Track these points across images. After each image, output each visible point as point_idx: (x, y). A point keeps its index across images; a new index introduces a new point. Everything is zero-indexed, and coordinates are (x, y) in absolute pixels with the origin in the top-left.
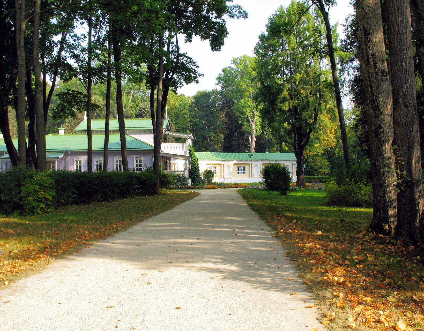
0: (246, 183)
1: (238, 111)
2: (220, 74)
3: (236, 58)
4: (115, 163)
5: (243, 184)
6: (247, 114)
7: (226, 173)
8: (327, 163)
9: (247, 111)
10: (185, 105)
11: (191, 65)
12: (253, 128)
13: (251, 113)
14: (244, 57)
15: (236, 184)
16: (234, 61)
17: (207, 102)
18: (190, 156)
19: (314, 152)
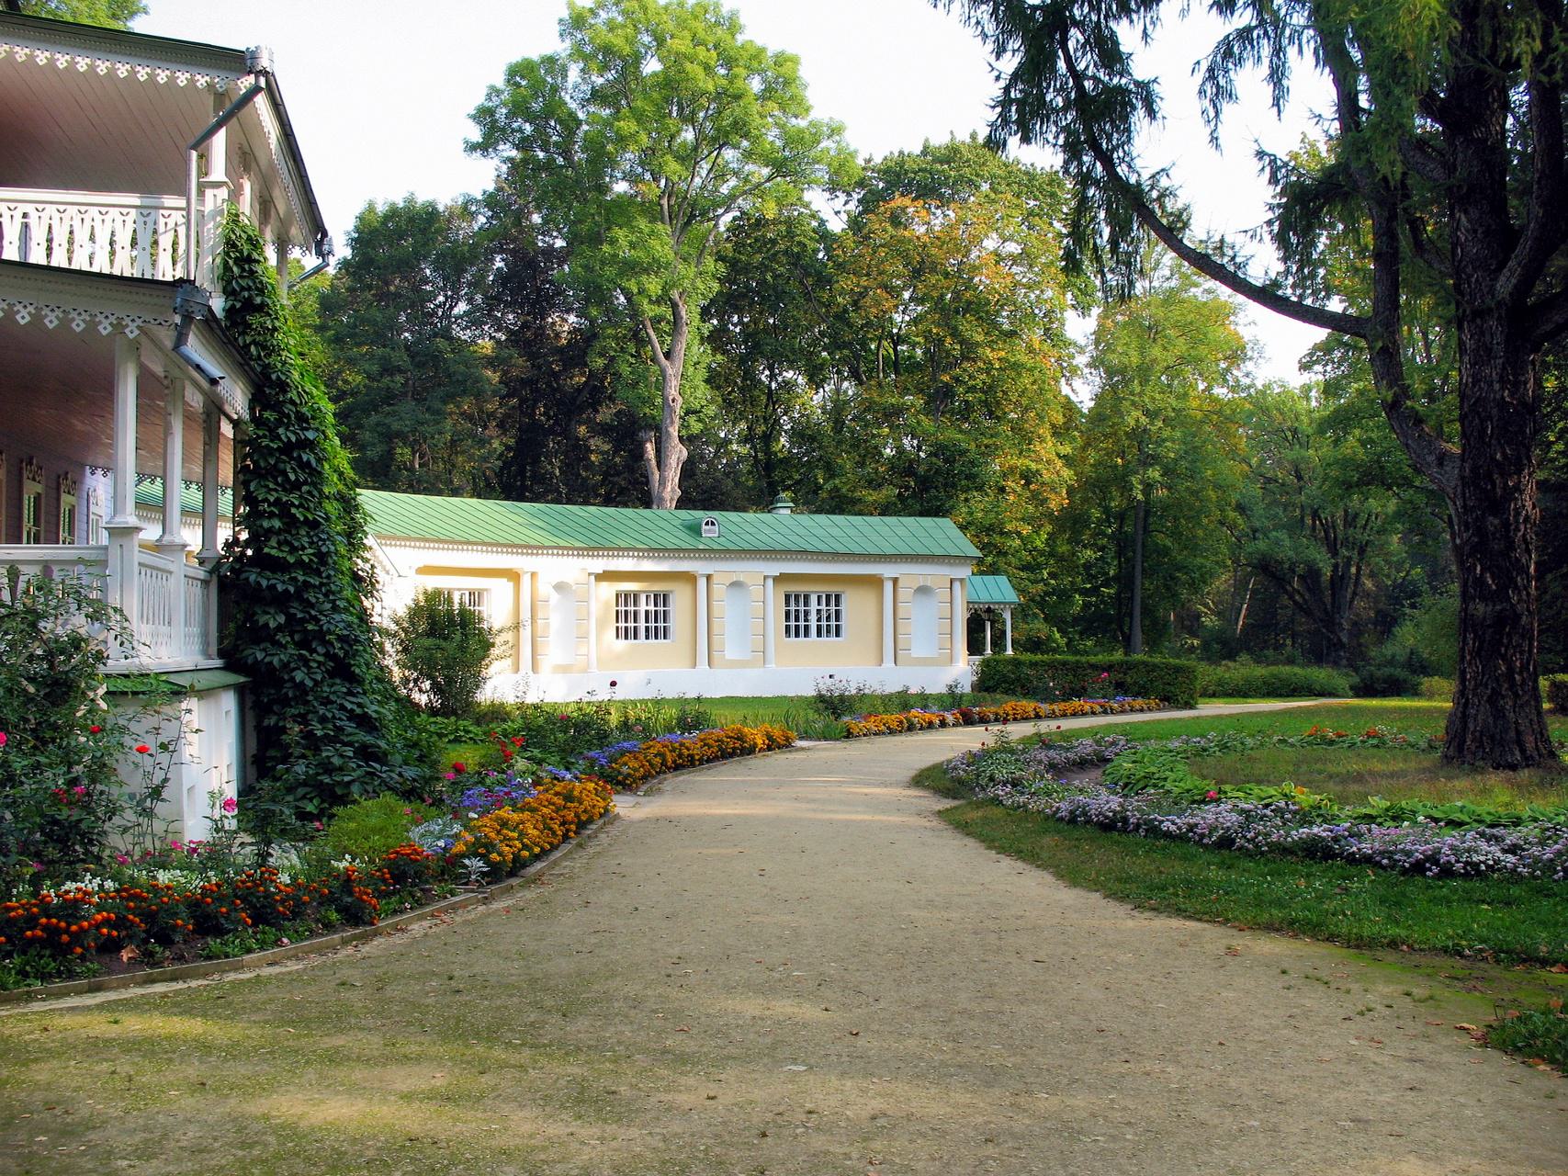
12: (673, 392)
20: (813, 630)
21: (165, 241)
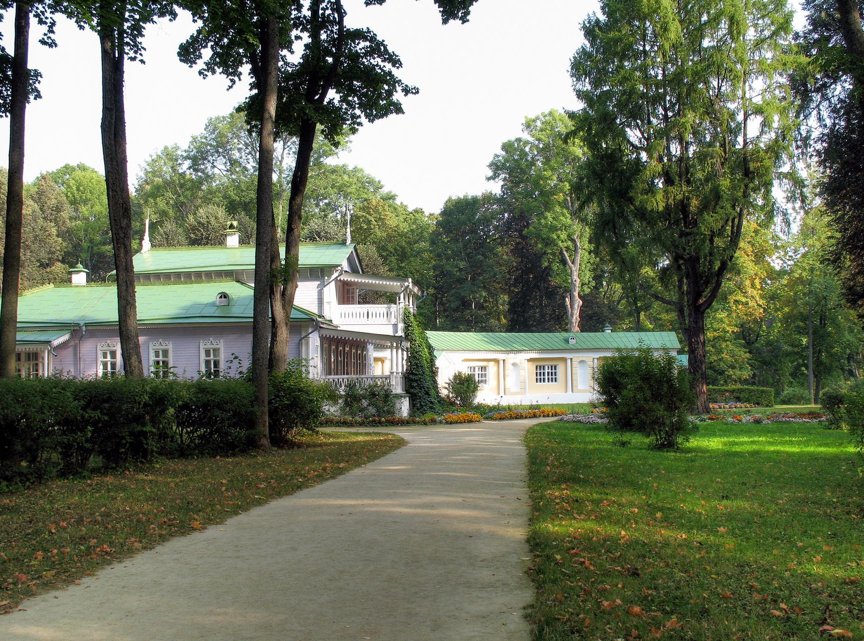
0: (557, 405)
1: (538, 236)
2: (497, 156)
3: (533, 117)
4: (203, 357)
5: (550, 408)
6: (560, 244)
7: (511, 382)
8: (744, 355)
9: (558, 237)
10: (422, 233)
11: (379, 60)
12: (575, 277)
13: (570, 243)
14: (550, 114)
15: (532, 407)
16: (528, 125)
17: (470, 220)
18: (408, 336)
19: (715, 331)
20: (547, 380)
21: (393, 313)
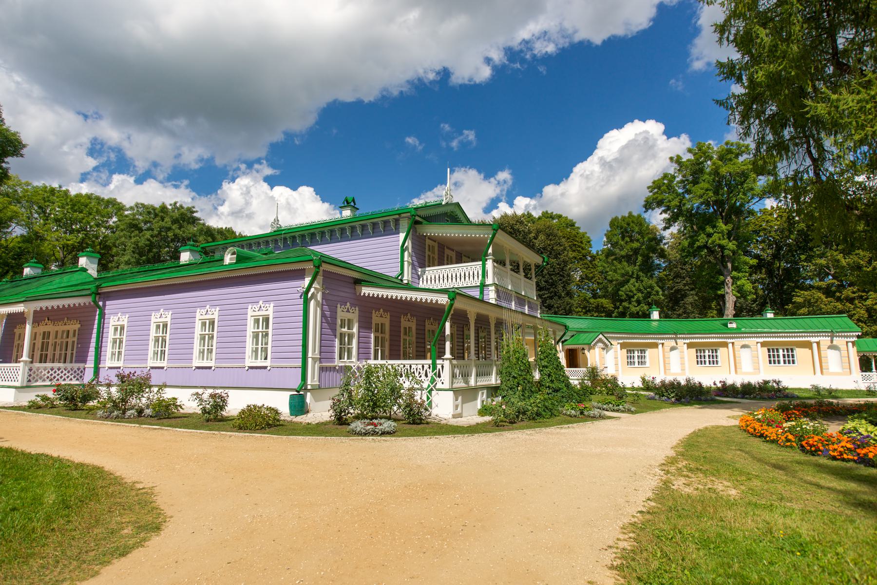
20: (782, 361)
